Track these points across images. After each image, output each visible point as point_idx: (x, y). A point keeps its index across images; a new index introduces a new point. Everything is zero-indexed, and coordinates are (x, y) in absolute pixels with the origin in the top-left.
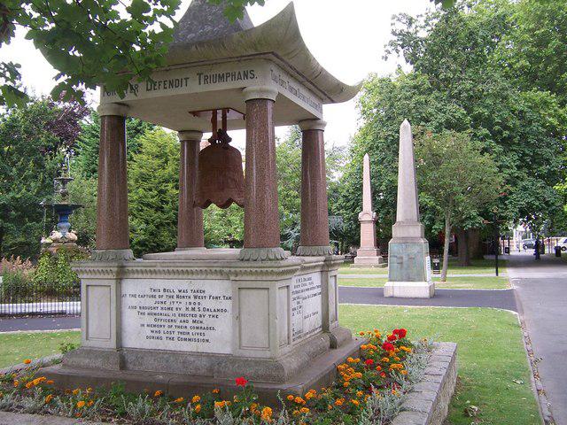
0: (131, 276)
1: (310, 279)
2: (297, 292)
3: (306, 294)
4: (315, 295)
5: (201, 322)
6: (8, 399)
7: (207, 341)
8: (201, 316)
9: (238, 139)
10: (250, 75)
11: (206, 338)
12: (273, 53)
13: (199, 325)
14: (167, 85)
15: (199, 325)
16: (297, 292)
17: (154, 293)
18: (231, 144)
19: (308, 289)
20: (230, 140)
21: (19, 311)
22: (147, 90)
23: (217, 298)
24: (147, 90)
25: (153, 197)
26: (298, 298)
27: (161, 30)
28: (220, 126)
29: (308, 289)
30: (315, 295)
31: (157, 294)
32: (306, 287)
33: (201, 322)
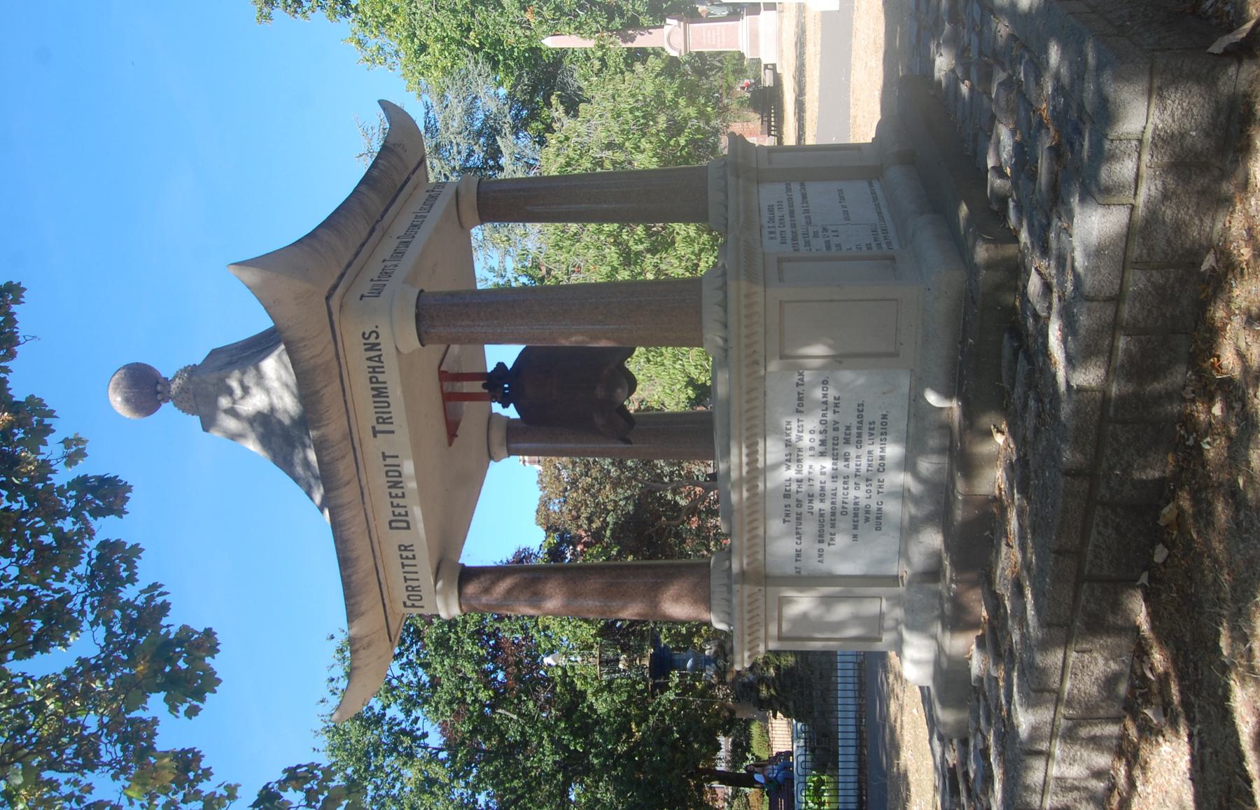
0: (760, 557)
1: (771, 209)
2: (795, 238)
3: (800, 218)
4: (804, 196)
5: (848, 428)
6: (1115, 800)
7: (884, 417)
8: (836, 429)
9: (502, 354)
10: (372, 340)
11: (878, 421)
12: (328, 298)
13: (854, 431)
14: (399, 492)
15: (854, 431)
16: (795, 238)
17: (794, 516)
18: (509, 365)
19: (792, 214)
20: (501, 366)
21: (852, 750)
22: (408, 528)
23: (800, 399)
24: (408, 528)
25: (597, 557)
26: (806, 234)
27: (1037, 808)
28: (477, 387)
29: (792, 214)
30: (804, 196)
31: (794, 510)
32: (787, 218)
33: (848, 428)
